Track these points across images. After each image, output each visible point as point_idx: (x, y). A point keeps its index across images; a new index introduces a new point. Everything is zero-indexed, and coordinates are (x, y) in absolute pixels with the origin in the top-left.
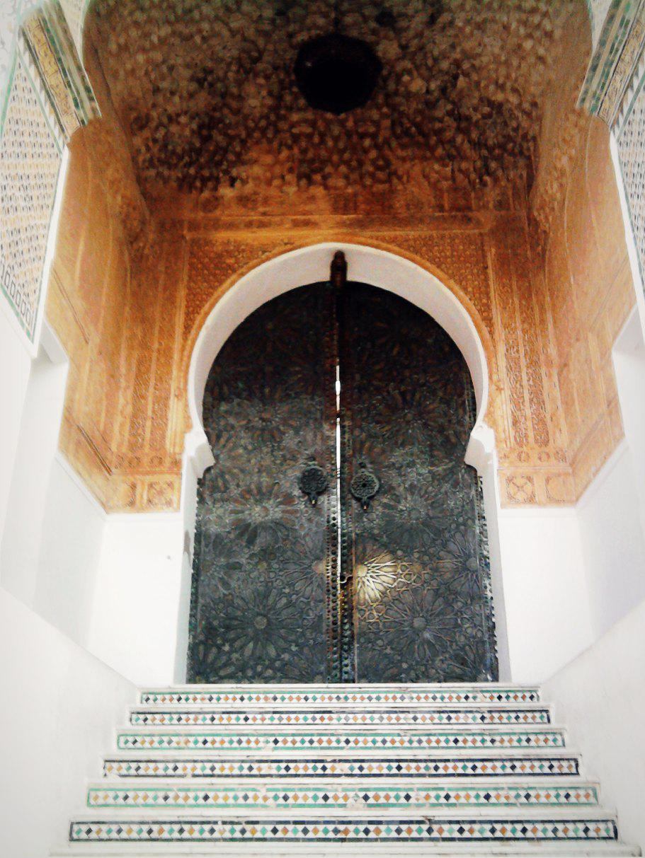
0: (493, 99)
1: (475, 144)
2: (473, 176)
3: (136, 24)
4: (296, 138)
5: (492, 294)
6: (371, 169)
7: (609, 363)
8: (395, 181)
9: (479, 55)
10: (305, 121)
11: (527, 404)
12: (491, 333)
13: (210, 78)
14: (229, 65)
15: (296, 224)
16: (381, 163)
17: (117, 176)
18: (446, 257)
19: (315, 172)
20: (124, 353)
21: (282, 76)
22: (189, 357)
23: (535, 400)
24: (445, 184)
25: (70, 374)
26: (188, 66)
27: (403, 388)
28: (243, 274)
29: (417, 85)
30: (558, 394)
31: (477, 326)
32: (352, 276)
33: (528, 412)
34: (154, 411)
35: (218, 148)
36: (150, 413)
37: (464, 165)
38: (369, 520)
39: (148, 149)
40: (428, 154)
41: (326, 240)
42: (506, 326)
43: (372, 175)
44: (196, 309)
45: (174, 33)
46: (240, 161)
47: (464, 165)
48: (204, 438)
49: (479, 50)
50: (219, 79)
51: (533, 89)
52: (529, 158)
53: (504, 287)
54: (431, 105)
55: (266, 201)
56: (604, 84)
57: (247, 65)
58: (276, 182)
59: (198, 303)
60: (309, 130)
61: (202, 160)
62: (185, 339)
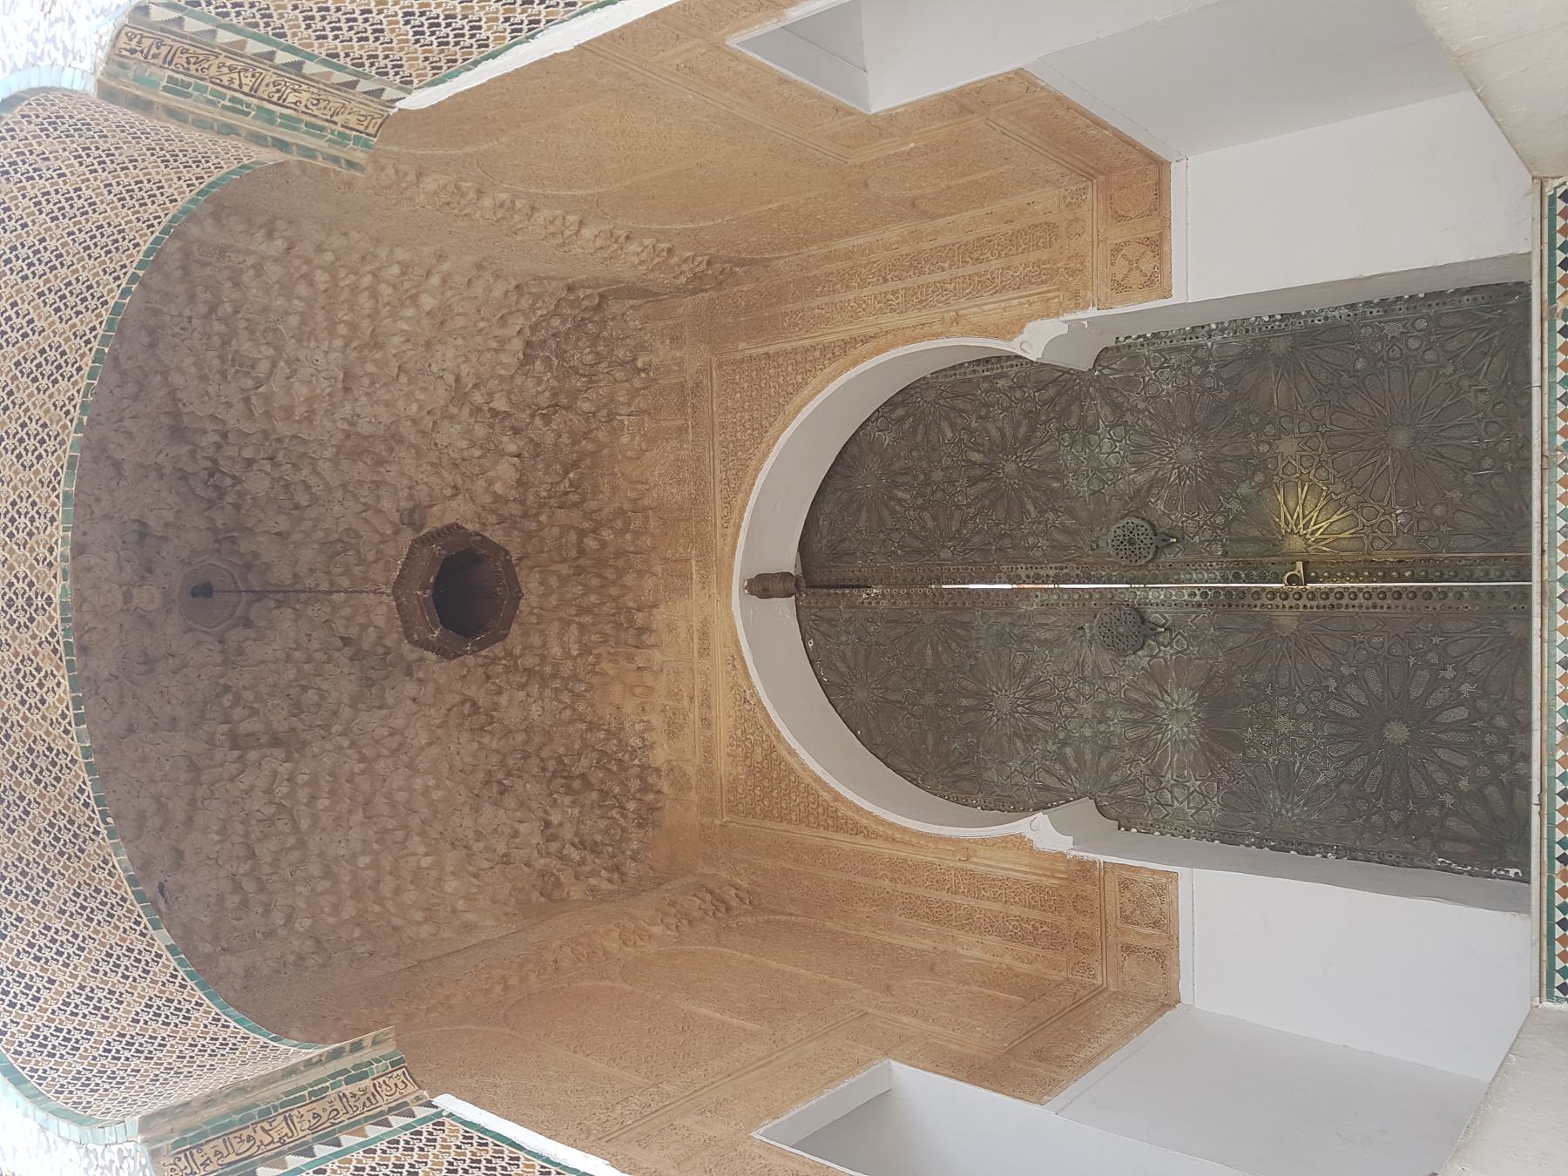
0: (521, 355)
1: (590, 381)
2: (637, 383)
3: (398, 891)
4: (586, 650)
5: (806, 343)
6: (628, 537)
7: (891, 116)
8: (646, 502)
9: (458, 379)
10: (560, 635)
11: (983, 267)
12: (865, 340)
13: (500, 775)
14: (482, 746)
15: (705, 651)
16: (619, 523)
17: (615, 934)
18: (752, 419)
19: (631, 622)
20: (900, 940)
21: (500, 669)
22: (905, 830)
23: (976, 255)
24: (648, 424)
25: (909, 1060)
26: (476, 810)
27: (963, 481)
28: (778, 735)
29: (506, 471)
30: (967, 215)
31: (855, 363)
32: (787, 560)
33: (996, 264)
34: (995, 900)
35: (600, 765)
36: (997, 907)
37: (622, 397)
38: (1197, 534)
39: (593, 873)
40: (605, 452)
41: (728, 607)
42: (855, 316)
43: (637, 535)
44: (831, 815)
45: (422, 834)
46: (616, 734)
47: (622, 397)
48: (1041, 818)
49: (450, 379)
50: (503, 763)
51: (498, 292)
52: (601, 296)
53: (796, 325)
54: (537, 448)
55: (675, 696)
56: (313, 126)
57: (479, 718)
58: (649, 681)
59: (820, 810)
60: (573, 628)
61: (617, 790)
62: (877, 835)
